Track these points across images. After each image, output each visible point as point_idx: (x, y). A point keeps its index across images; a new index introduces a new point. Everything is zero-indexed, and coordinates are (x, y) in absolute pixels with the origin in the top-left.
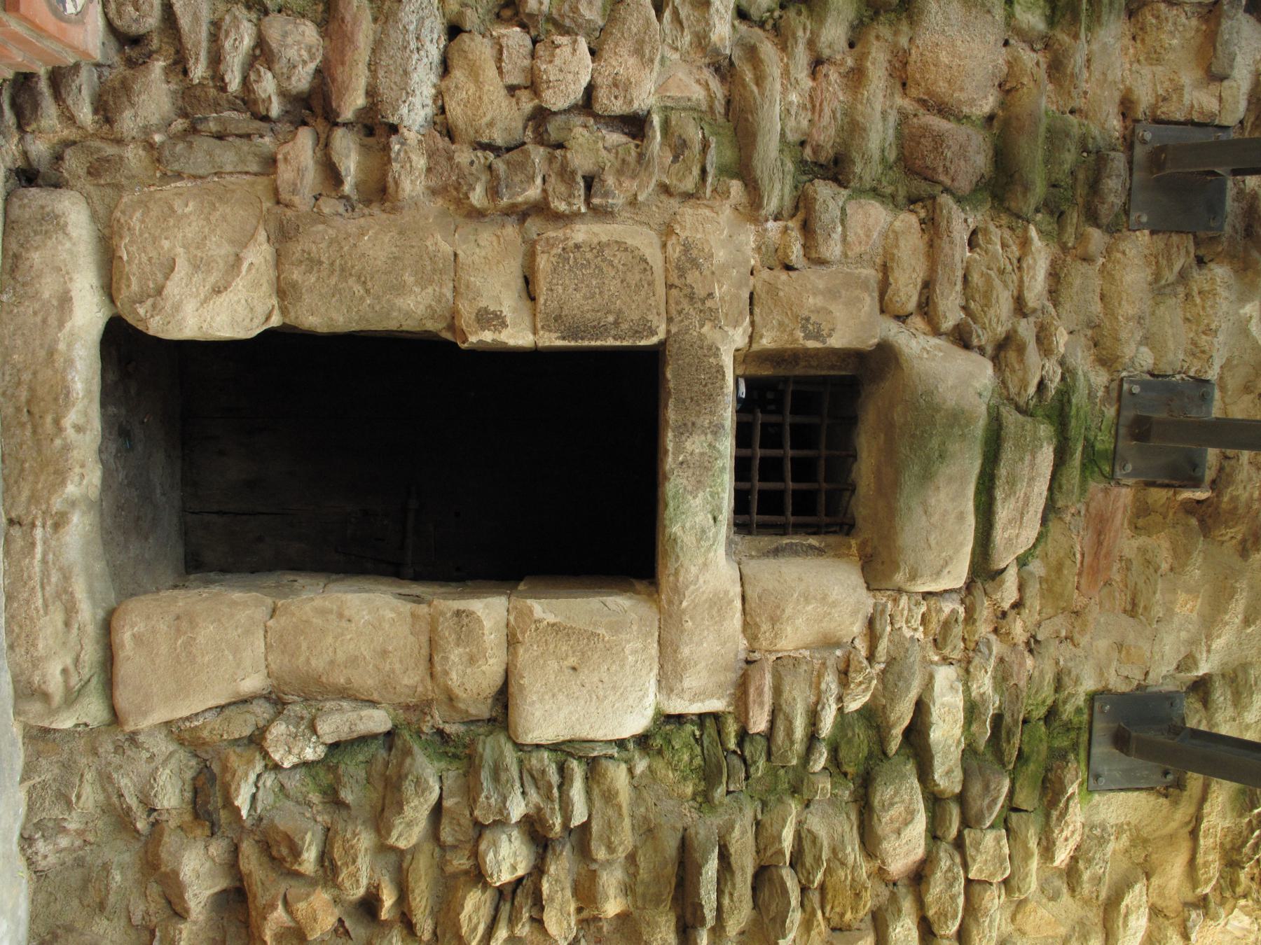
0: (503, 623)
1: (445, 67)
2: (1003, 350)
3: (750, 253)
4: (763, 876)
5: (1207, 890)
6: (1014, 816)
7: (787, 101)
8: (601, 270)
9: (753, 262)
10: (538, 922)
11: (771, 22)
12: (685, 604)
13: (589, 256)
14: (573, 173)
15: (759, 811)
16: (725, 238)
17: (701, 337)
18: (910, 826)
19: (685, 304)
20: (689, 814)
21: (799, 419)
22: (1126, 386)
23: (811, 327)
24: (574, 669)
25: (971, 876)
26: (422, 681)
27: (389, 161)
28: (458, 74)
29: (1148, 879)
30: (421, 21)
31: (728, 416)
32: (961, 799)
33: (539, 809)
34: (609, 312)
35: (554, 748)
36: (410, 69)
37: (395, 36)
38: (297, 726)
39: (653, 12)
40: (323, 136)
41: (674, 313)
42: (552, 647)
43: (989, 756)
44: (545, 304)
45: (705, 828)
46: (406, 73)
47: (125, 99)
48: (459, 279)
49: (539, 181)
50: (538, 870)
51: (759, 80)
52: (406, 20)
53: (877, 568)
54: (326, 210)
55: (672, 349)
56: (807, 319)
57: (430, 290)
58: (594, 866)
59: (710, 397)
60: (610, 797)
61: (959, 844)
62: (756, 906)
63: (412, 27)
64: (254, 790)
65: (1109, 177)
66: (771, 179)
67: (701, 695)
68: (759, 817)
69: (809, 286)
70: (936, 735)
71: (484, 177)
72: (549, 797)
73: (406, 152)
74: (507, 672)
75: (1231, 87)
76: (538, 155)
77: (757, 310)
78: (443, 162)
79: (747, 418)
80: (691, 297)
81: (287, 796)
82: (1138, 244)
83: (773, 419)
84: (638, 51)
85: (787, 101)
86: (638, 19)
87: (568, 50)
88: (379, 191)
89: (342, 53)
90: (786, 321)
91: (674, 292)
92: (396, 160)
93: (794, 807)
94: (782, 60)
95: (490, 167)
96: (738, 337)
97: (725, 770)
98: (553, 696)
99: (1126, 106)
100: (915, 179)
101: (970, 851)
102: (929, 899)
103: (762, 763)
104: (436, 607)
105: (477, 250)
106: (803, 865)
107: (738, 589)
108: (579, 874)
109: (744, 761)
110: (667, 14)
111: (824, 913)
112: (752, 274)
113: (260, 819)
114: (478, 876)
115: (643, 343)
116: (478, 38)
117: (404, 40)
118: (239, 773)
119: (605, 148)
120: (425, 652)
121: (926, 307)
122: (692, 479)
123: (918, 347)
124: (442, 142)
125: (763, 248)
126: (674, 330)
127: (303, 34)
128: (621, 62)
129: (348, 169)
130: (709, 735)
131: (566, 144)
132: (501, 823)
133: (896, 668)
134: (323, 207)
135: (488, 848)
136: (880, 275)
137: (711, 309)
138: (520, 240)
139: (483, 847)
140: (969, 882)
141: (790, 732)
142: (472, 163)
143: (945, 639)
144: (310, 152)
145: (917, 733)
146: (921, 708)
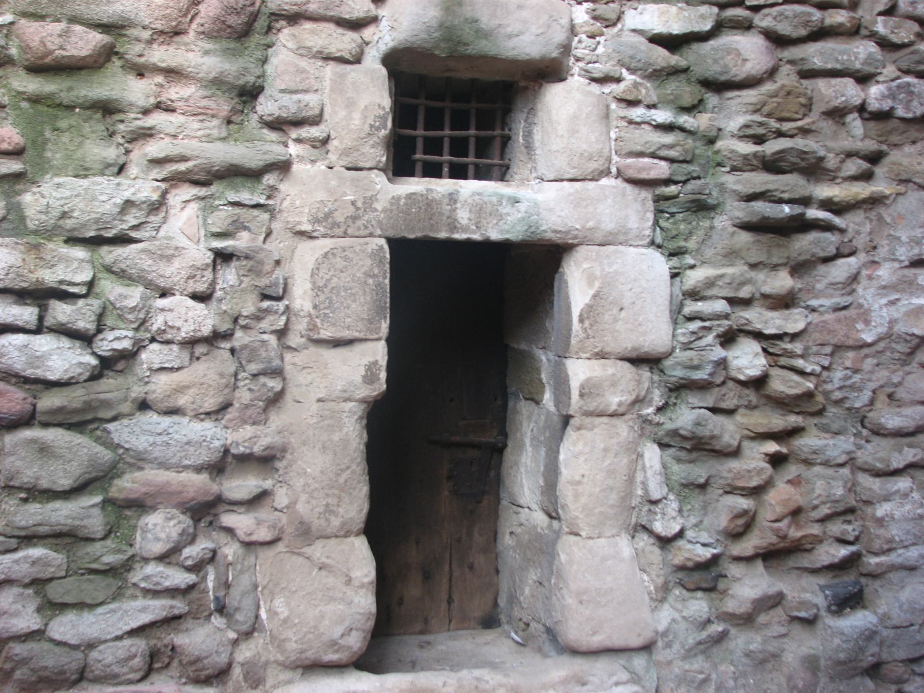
0: (587, 362)
1: (174, 411)
4: (772, 165)
7: (192, 135)
8: (333, 288)
9: (323, 167)
10: (794, 337)
11: (126, 145)
12: (578, 227)
13: (322, 297)
14: (260, 310)
15: (723, 169)
17: (384, 211)
18: (742, 52)
19: (359, 223)
20: (722, 222)
21: (421, 124)
23: (377, 124)
24: (622, 309)
26: (626, 422)
28: (182, 401)
30: (144, 432)
31: (443, 186)
33: (718, 336)
34: (365, 283)
35: (675, 322)
36: (185, 440)
37: (157, 453)
38: (655, 513)
40: (228, 507)
41: (367, 232)
42: (607, 326)
44: (360, 332)
45: (738, 211)
46: (188, 443)
47: (205, 661)
48: (338, 398)
50: (758, 336)
51: (183, 159)
52: (146, 444)
53: (549, 71)
55: (391, 233)
56: (371, 126)
57: (346, 420)
59: (428, 204)
60: (710, 283)
62: (790, 172)
63: (151, 439)
64: (699, 545)
66: (265, 153)
68: (728, 169)
69: (344, 123)
70: (676, 28)
72: (709, 329)
73: (245, 441)
74: (622, 359)
76: (240, 338)
77: (361, 165)
78: (249, 412)
79: (419, 167)
80: (355, 218)
81: (701, 522)
83: (420, 144)
84: (169, 258)
85: (192, 135)
86: (141, 259)
88: (266, 461)
89: (171, 494)
90: (371, 142)
91: (350, 231)
92: (252, 448)
94: (162, 138)
95: (255, 376)
96: (379, 180)
97: (699, 196)
98: (640, 325)
103: (691, 168)
104: (576, 412)
105: (315, 384)
106: (764, 135)
108: (762, 306)
109: (688, 180)
110: (134, 234)
111: (800, 119)
112: (331, 168)
113: (718, 540)
114: (759, 383)
115: (388, 256)
117: (161, 445)
118: (687, 555)
119: (240, 285)
120: (605, 419)
121: (356, 25)
122: (489, 219)
124: (231, 414)
125: (312, 158)
126: (379, 232)
127: (155, 525)
128: (172, 272)
129: (256, 486)
130: (668, 207)
131: (235, 316)
132: (722, 363)
133: (627, 60)
134: (283, 505)
136: (331, 63)
137: (364, 203)
138: (306, 351)
141: (671, 147)
142: (250, 389)
143: (606, 20)
144: (241, 517)
145: (671, 43)
146: (658, 40)
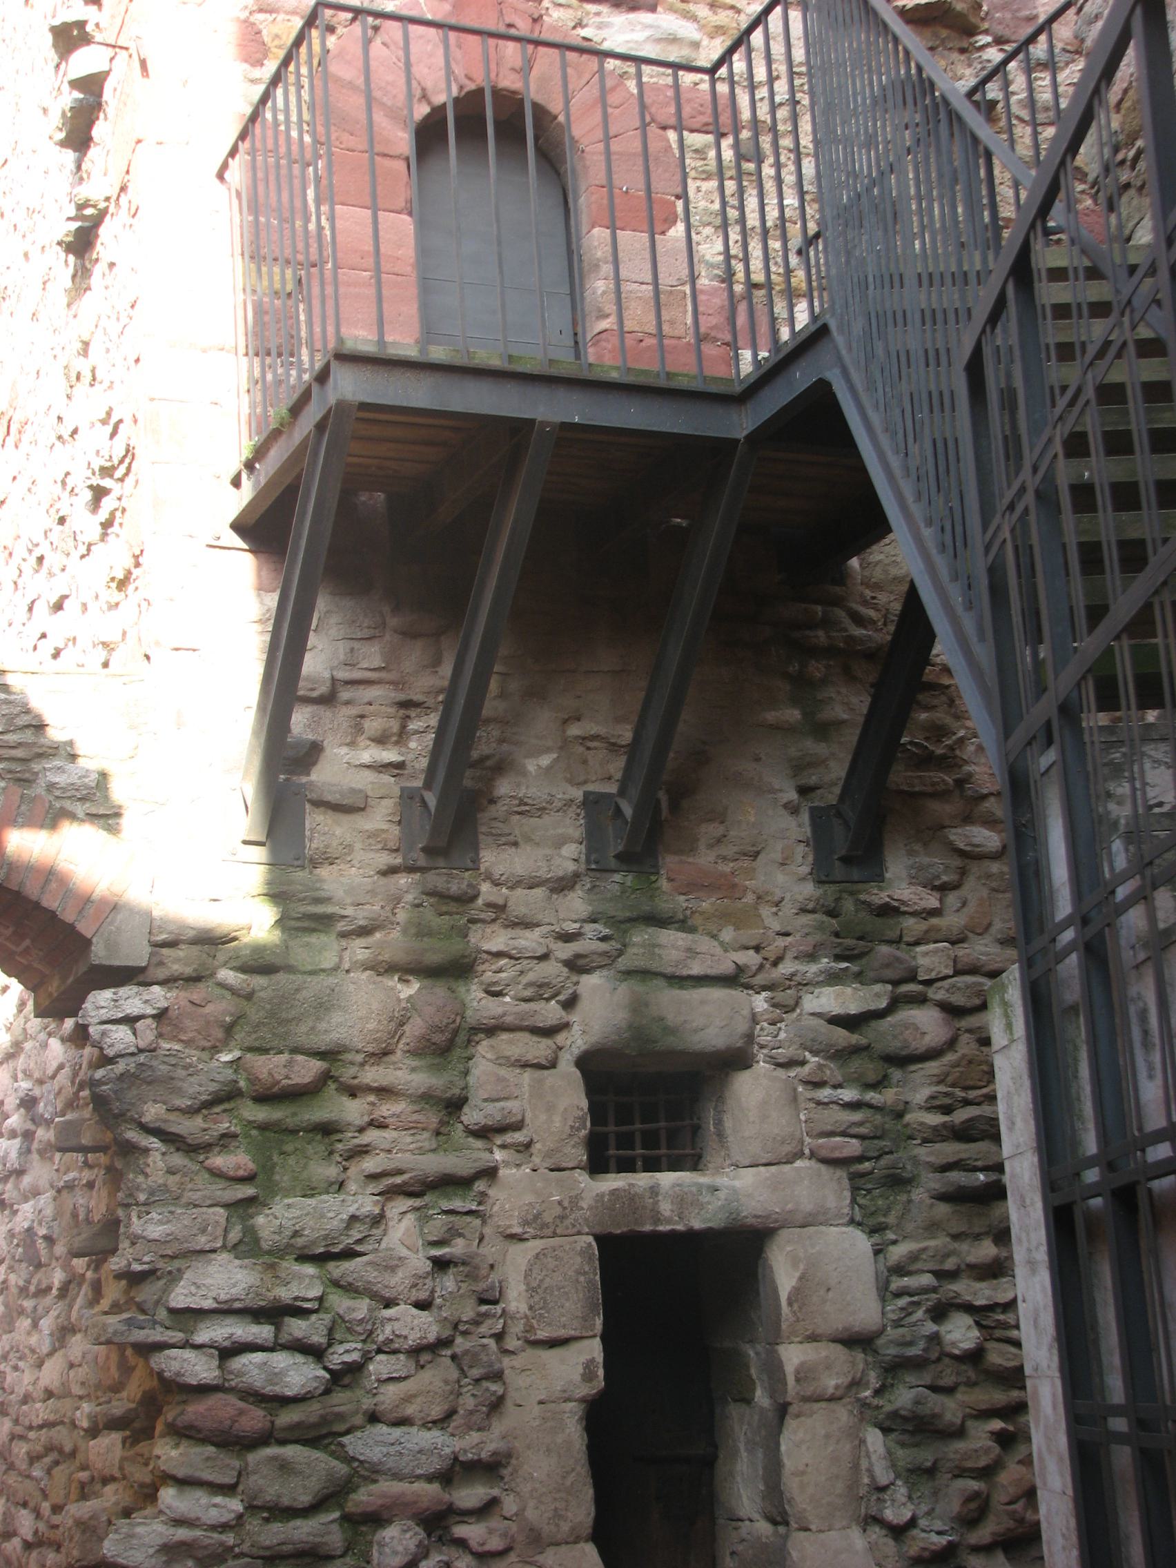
0: (800, 1346)
2: (577, 966)
3: (521, 1172)
5: (950, 781)
6: (905, 939)
13: (537, 1298)
14: (479, 1314)
16: (517, 1190)
19: (567, 1222)
22: (593, 866)
24: (829, 1290)
25: (950, 972)
27: (480, 1461)
28: (410, 1410)
29: (945, 827)
31: (642, 1180)
32: (896, 983)
35: (883, 1300)
36: (417, 1448)
37: (390, 1463)
38: (885, 1501)
39: (359, 1259)
41: (575, 1230)
43: (864, 961)
45: (932, 1182)
46: (420, 1452)
49: (485, 1341)
50: (969, 1308)
53: (736, 1059)
54: (514, 1509)
55: (598, 1230)
56: (572, 1127)
58: (963, 1267)
60: (914, 1257)
61: (928, 983)
63: (385, 1450)
65: (448, 889)
67: (832, 1191)
68: (919, 1141)
70: (853, 1009)
71: (485, 1384)
75: (373, 789)
77: (564, 1165)
80: (562, 1218)
81: (933, 1509)
82: (492, 859)
83: (612, 1141)
84: (393, 1269)
87: (397, 1325)
93: (908, 1118)
99: (391, 871)
100: (448, 1044)
101: (933, 975)
102: (969, 1005)
107: (762, 1169)
110: (358, 1248)
114: (975, 1356)
116: (380, 1398)
118: (922, 1545)
120: (823, 1404)
121: (548, 1032)
123: (576, 1041)
124: (457, 1421)
127: (392, 1538)
128: (397, 1282)
135: (957, 1348)
136: (528, 1069)
139: (957, 1352)
140: (957, 973)
141: (861, 1124)
142: (473, 1395)
144: (472, 1527)
